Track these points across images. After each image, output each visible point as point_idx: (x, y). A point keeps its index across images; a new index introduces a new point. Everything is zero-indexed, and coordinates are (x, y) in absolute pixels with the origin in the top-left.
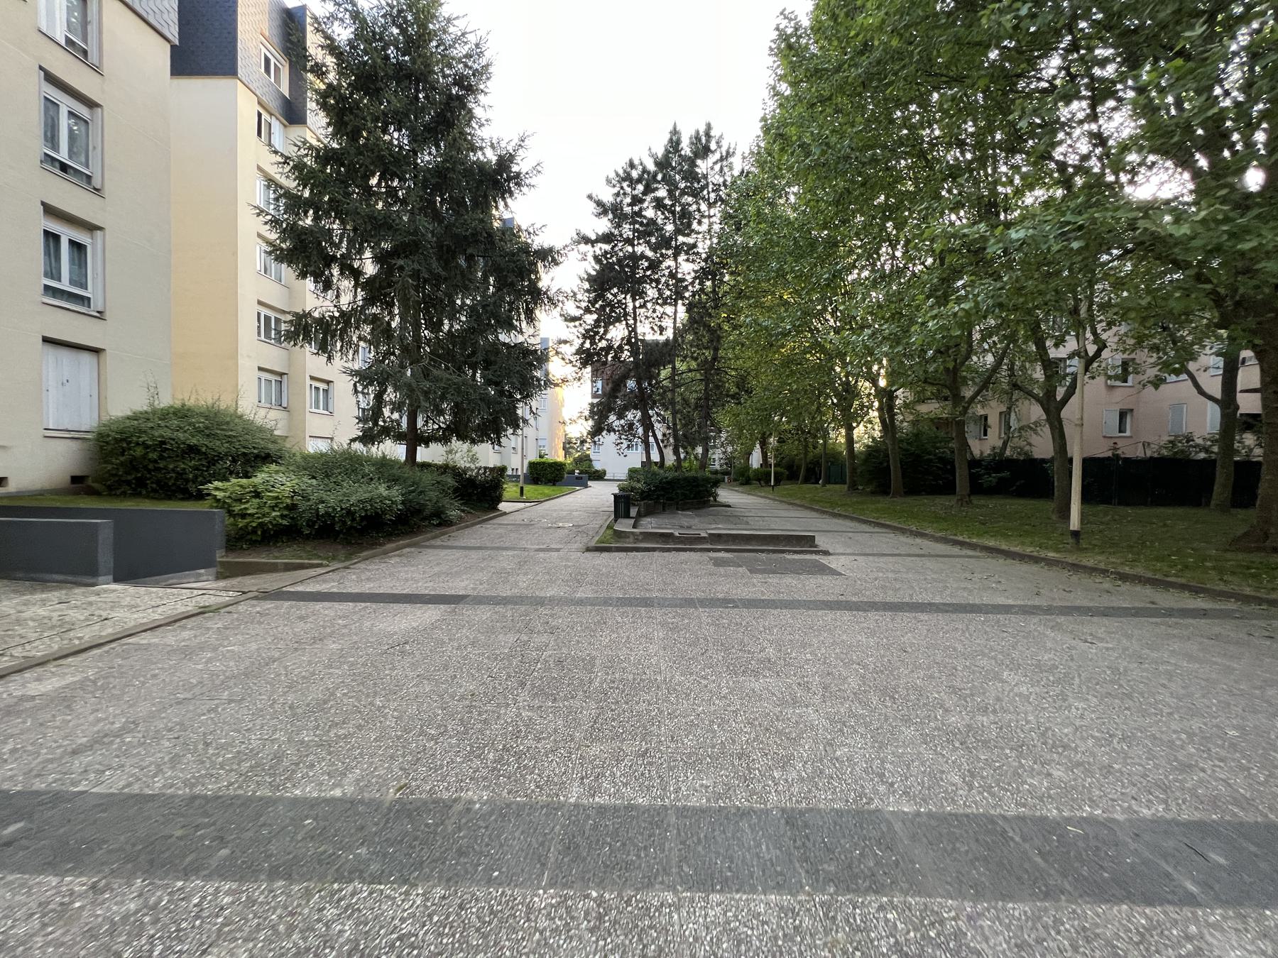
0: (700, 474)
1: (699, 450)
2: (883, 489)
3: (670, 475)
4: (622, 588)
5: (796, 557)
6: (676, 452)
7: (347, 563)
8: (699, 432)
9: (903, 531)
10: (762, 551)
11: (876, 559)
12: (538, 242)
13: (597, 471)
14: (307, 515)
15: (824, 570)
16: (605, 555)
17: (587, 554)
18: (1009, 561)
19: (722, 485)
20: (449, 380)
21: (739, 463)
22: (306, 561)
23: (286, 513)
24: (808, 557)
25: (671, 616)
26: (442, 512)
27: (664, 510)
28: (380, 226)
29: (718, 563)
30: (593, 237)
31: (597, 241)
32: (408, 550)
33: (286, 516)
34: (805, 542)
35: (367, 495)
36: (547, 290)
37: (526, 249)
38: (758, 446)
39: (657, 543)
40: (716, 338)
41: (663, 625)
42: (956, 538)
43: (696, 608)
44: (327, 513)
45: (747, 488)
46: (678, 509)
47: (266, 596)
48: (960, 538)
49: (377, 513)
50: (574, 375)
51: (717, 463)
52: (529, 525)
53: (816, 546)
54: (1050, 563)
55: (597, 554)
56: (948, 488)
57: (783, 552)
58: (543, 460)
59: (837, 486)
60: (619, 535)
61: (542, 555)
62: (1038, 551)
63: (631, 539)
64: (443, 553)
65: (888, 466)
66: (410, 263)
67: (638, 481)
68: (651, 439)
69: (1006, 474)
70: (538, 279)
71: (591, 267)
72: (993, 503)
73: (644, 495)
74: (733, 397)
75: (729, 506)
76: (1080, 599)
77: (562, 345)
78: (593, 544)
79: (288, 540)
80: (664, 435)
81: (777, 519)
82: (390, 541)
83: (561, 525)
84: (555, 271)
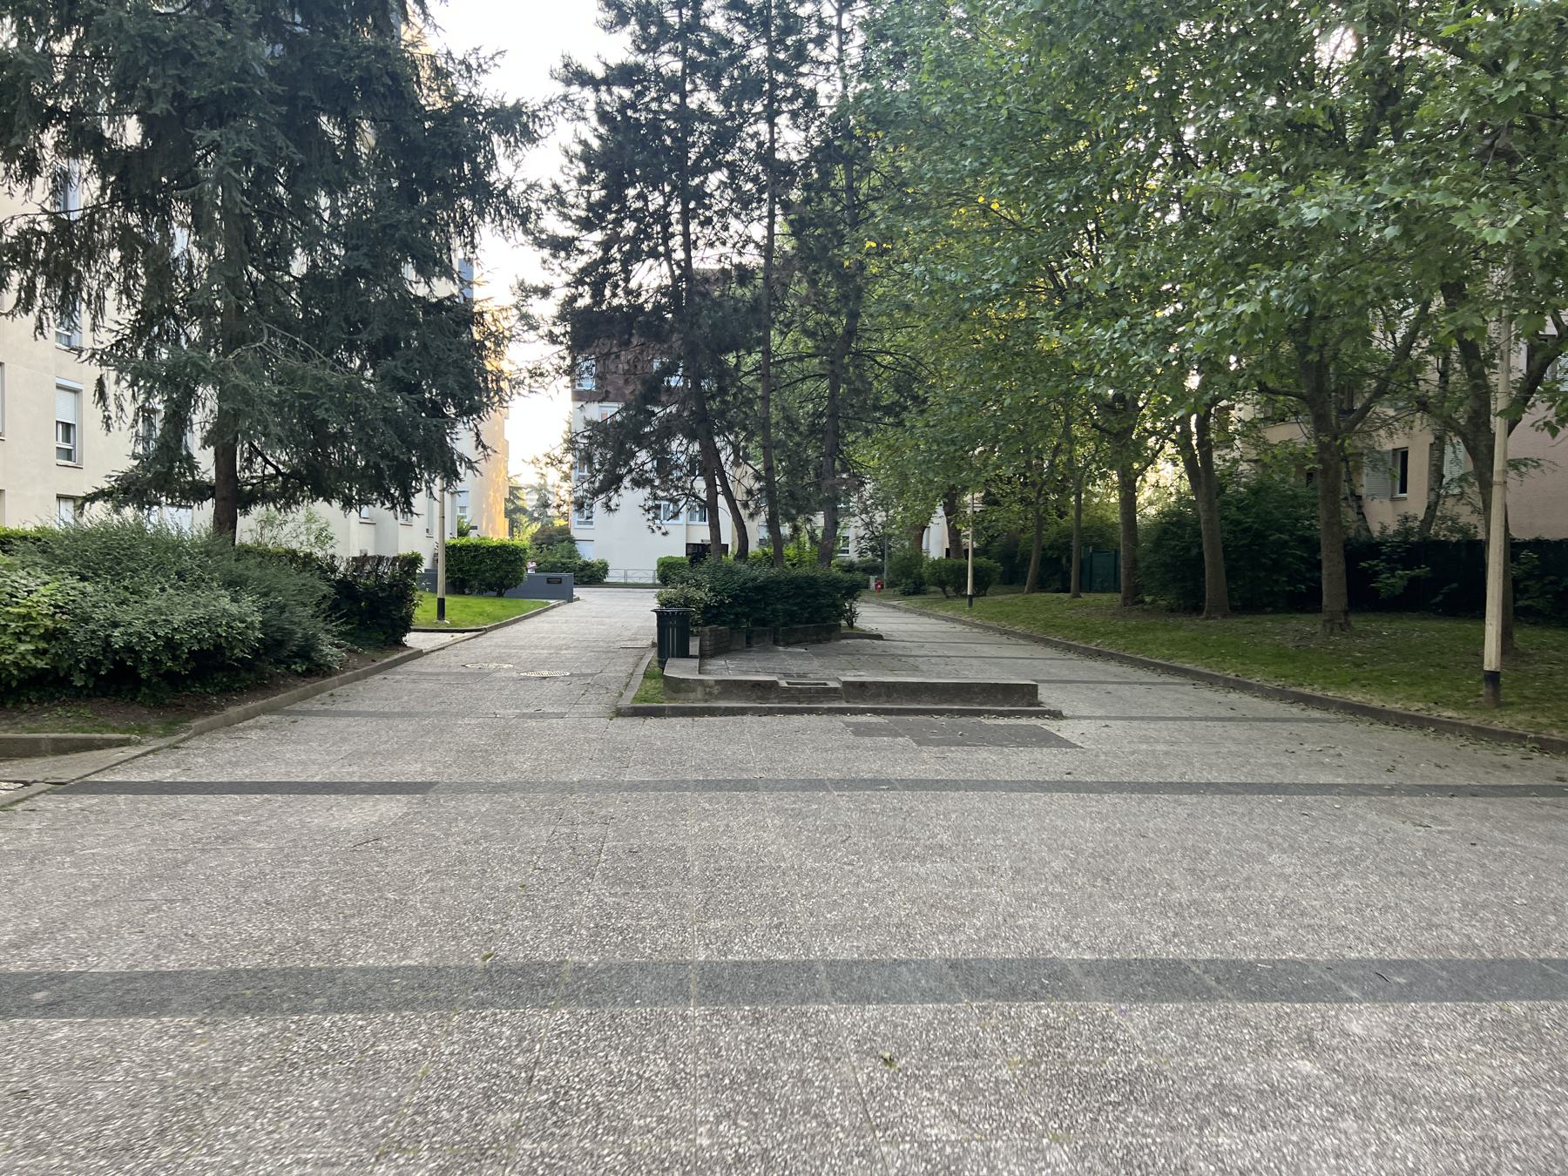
0: (820, 572)
1: (820, 520)
2: (1192, 603)
3: (763, 573)
4: (698, 768)
5: (1002, 721)
6: (772, 525)
7: (172, 740)
8: (818, 486)
9: (1211, 681)
10: (941, 713)
11: (1144, 725)
12: (494, 89)
13: (587, 565)
14: (86, 652)
15: (1048, 740)
16: (652, 722)
17: (619, 721)
18: (1379, 726)
19: (865, 595)
20: (318, 379)
21: (900, 546)
22: (98, 735)
23: (42, 645)
24: (1024, 721)
25: (789, 801)
26: (313, 648)
27: (749, 644)
28: (167, 55)
29: (859, 731)
30: (600, 73)
31: (608, 82)
32: (263, 719)
33: (45, 652)
34: (1021, 697)
35: (201, 612)
36: (508, 187)
37: (464, 109)
38: (940, 511)
39: (748, 699)
40: (852, 287)
41: (778, 811)
42: (1301, 690)
43: (828, 791)
44: (129, 648)
45: (916, 601)
46: (776, 643)
47: (61, 787)
48: (1307, 691)
49: (218, 647)
50: (556, 361)
51: (852, 547)
52: (464, 677)
53: (1039, 704)
54: (1443, 728)
55: (638, 721)
56: (1306, 601)
57: (979, 713)
58: (464, 541)
59: (1105, 597)
60: (676, 687)
61: (533, 723)
62: (1429, 709)
63: (699, 693)
64: (342, 722)
65: (1201, 554)
66: (232, 135)
67: (699, 586)
68: (722, 501)
69: (1422, 571)
70: (491, 162)
71: (591, 132)
72: (1388, 628)
73: (711, 614)
74: (888, 410)
75: (879, 637)
76: (1425, 773)
77: (534, 299)
78: (626, 702)
79: (40, 701)
80: (749, 492)
81: (974, 662)
82: (230, 702)
83: (546, 673)
84: (529, 153)
